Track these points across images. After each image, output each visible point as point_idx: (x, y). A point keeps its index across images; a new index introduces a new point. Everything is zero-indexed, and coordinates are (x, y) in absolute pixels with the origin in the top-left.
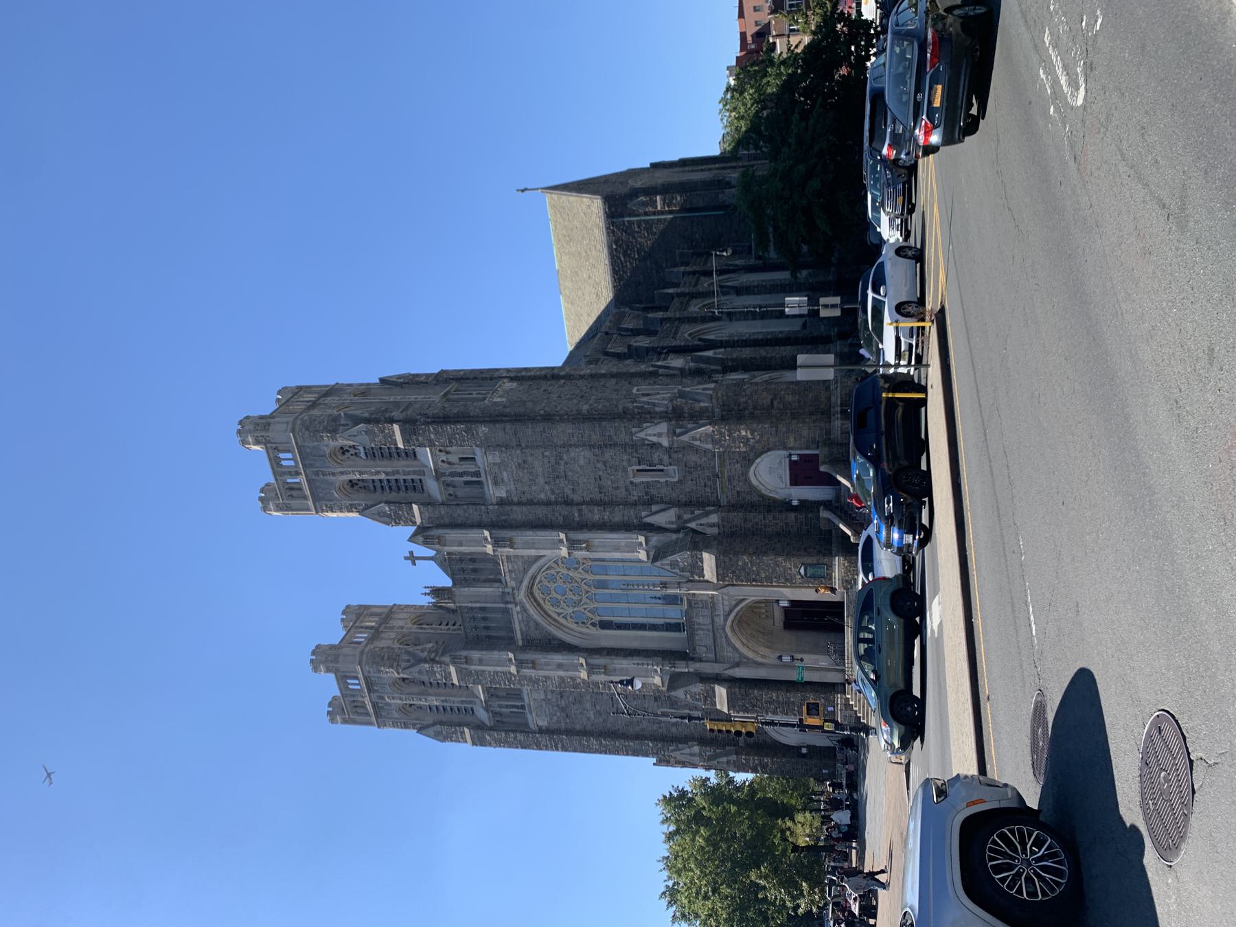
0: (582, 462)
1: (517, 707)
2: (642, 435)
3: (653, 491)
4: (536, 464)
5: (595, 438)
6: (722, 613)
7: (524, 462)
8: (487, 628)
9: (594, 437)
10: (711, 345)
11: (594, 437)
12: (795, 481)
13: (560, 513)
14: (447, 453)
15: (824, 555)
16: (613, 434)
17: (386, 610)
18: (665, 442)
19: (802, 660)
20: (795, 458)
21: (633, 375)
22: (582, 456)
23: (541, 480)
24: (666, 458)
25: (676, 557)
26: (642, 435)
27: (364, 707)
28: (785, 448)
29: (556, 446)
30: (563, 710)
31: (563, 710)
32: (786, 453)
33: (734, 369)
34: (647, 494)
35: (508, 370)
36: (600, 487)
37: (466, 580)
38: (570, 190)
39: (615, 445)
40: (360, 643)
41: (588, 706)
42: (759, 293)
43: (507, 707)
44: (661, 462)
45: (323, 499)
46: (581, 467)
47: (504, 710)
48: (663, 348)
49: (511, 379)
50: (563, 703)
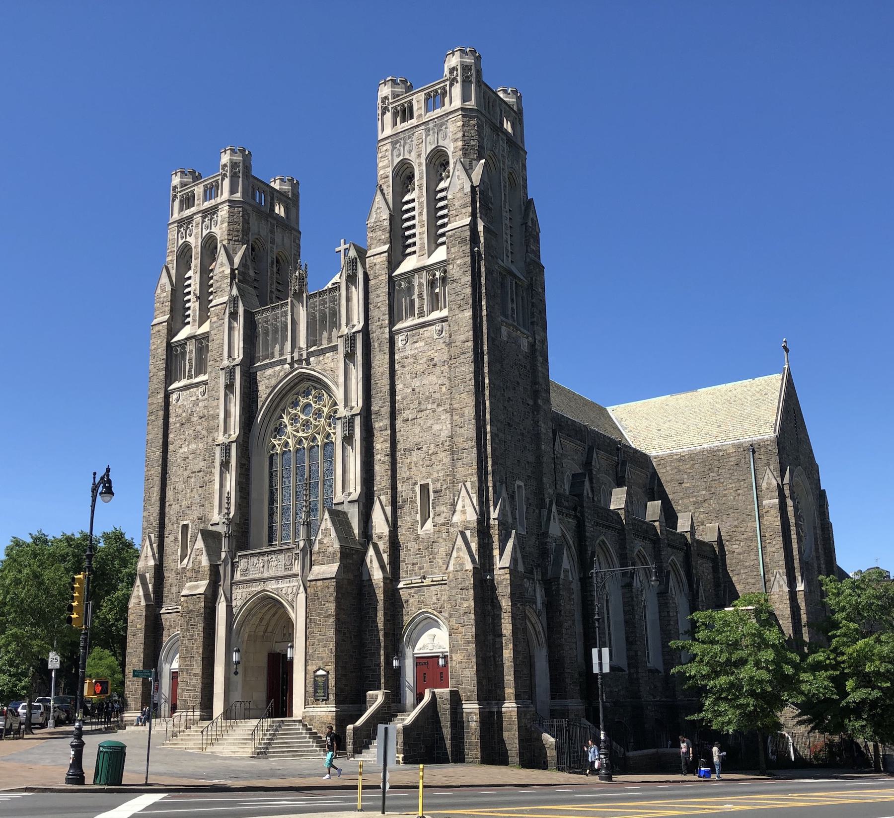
0: (436, 427)
2: (463, 493)
4: (433, 378)
7: (435, 365)
8: (266, 333)
10: (584, 563)
13: (380, 405)
16: (465, 461)
18: (457, 518)
19: (236, 673)
21: (540, 481)
22: (443, 428)
23: (416, 383)
25: (333, 534)
27: (188, 207)
30: (189, 420)
31: (189, 420)
33: (548, 592)
35: (544, 341)
38: (786, 401)
39: (454, 466)
40: (254, 198)
41: (193, 446)
42: (661, 618)
45: (394, 148)
49: (532, 346)
50: (194, 419)
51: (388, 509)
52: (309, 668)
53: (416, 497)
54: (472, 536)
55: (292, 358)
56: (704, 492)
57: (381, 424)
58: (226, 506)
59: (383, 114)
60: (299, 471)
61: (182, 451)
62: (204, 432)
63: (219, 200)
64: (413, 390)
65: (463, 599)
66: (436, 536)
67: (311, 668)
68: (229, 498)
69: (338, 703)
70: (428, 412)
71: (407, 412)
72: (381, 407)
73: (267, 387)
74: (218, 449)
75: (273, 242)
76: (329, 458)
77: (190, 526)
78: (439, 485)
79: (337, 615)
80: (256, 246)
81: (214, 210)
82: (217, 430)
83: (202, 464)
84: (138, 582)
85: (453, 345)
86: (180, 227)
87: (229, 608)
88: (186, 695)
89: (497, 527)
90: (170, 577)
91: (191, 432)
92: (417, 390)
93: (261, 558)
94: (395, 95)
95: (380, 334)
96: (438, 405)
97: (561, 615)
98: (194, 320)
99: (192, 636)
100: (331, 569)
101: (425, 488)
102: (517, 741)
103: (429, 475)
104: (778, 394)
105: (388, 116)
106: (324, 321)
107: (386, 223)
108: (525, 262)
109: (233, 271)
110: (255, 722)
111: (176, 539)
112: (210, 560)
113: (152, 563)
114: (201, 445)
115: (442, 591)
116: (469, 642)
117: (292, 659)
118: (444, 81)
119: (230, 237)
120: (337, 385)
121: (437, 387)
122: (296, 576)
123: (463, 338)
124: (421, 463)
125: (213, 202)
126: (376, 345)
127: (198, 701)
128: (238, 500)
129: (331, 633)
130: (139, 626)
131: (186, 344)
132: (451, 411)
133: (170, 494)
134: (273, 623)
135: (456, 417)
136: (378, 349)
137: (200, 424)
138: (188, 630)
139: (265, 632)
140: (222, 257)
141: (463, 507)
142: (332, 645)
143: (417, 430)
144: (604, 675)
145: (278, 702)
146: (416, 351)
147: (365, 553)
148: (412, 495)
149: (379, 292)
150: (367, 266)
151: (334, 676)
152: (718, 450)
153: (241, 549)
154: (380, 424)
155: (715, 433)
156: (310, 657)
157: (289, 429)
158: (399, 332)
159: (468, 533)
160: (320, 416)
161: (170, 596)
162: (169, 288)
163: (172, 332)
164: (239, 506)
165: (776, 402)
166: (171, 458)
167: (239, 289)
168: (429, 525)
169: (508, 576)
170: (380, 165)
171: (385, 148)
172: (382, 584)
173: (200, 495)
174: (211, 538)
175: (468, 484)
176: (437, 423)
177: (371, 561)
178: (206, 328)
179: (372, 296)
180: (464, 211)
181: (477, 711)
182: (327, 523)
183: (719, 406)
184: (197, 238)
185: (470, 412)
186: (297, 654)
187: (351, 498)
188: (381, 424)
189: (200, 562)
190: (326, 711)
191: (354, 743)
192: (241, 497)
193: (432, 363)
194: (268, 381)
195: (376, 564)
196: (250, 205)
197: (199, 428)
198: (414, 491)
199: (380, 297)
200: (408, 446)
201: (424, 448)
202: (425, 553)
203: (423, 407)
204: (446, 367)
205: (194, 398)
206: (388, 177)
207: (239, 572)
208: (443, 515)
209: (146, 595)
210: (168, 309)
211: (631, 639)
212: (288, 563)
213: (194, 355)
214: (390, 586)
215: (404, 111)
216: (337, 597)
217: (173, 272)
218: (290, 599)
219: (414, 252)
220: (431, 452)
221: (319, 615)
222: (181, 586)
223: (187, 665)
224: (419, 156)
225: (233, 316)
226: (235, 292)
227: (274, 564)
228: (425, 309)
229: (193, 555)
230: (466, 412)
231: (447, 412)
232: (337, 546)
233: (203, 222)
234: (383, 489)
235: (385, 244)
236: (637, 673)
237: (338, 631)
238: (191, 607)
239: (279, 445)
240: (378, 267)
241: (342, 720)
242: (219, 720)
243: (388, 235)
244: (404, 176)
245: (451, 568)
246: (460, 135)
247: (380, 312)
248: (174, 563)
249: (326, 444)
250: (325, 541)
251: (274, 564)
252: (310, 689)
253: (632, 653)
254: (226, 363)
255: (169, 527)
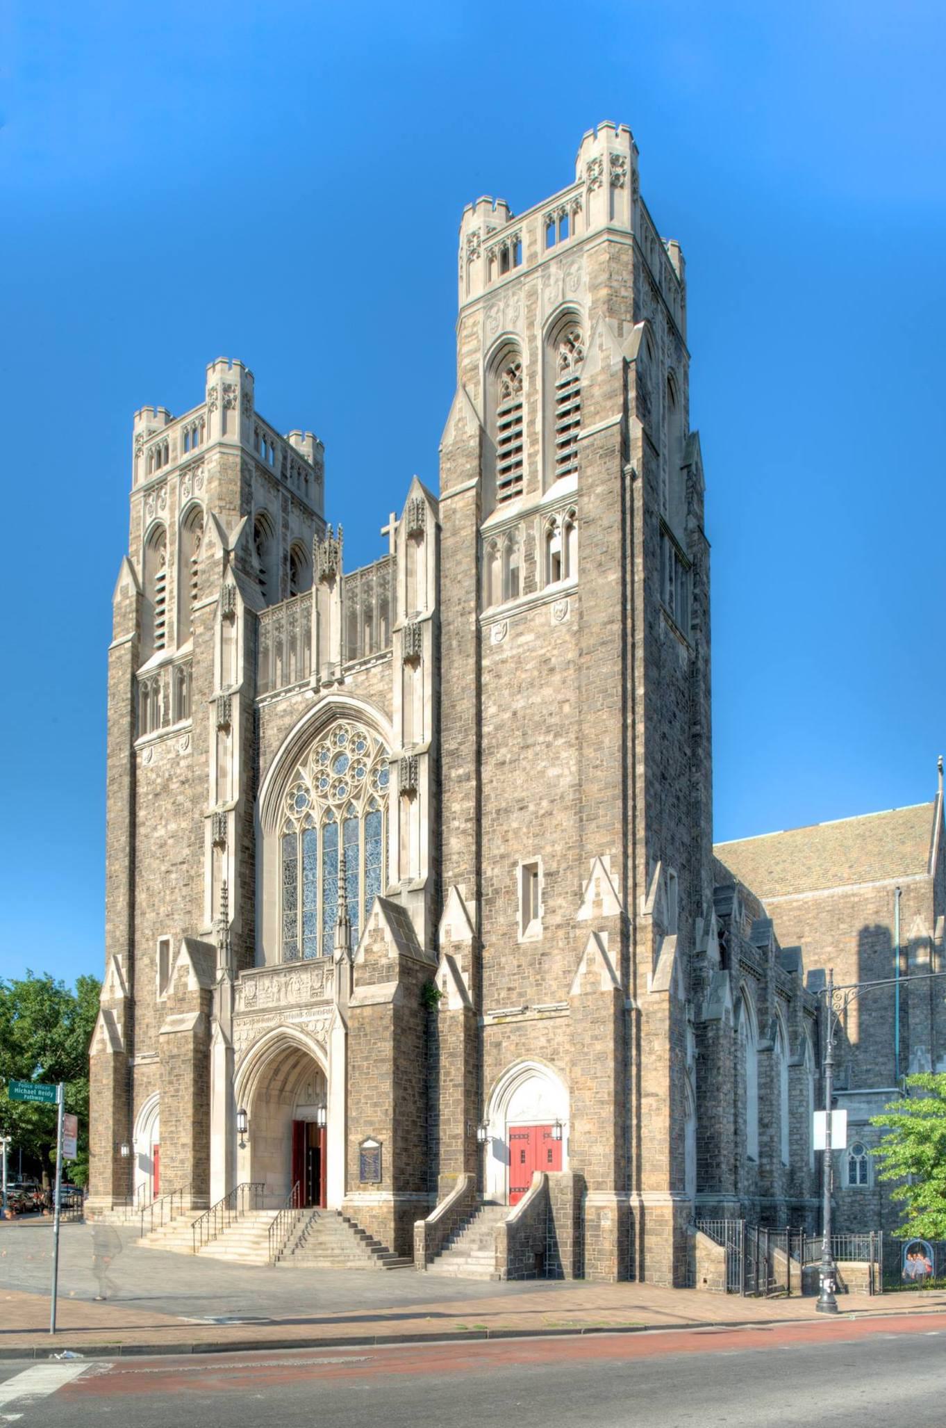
0: (552, 772)
1: (166, 713)
4: (548, 692)
5: (593, 789)
6: (304, 1019)
7: (552, 670)
9: (595, 787)
11: (595, 787)
12: (810, 973)
13: (458, 741)
14: (569, 528)
16: (602, 821)
17: (316, 509)
18: (586, 913)
20: (555, 1133)
22: (563, 772)
23: (519, 703)
24: (557, 919)
25: (388, 935)
26: (598, 872)
28: (573, 1116)
29: (580, 723)
30: (165, 788)
31: (165, 788)
34: (497, 892)
36: (507, 811)
41: (173, 826)
44: (551, 911)
46: (542, 773)
47: (161, 696)
48: (728, 941)
50: (174, 786)
51: (471, 906)
52: (351, 1137)
53: (515, 883)
54: (611, 940)
55: (318, 680)
56: (829, 949)
57: (461, 771)
58: (222, 901)
59: (470, 261)
60: (330, 860)
61: (156, 835)
62: (188, 805)
63: (205, 446)
64: (515, 714)
65: (595, 1038)
66: (548, 945)
68: (225, 890)
69: (399, 1188)
70: (538, 748)
72: (460, 744)
73: (279, 730)
74: (208, 823)
75: (286, 526)
78: (555, 865)
79: (395, 1059)
80: (261, 529)
82: (207, 799)
83: (186, 851)
84: (101, 1020)
85: (586, 631)
86: (147, 496)
87: (230, 1051)
88: (170, 1173)
89: (650, 928)
90: (144, 1014)
91: (169, 806)
92: (520, 714)
93: (276, 978)
94: (491, 230)
95: (460, 623)
96: (555, 736)
98: (171, 638)
99: (177, 1091)
100: (387, 990)
102: (670, 1250)
103: (537, 850)
105: (479, 265)
106: (370, 616)
107: (474, 443)
108: (686, 529)
109: (227, 553)
110: (274, 1213)
111: (152, 961)
112: (200, 982)
113: (120, 994)
114: (184, 825)
115: (554, 1027)
116: (602, 1102)
117: (325, 1127)
118: (578, 186)
119: (223, 503)
120: (389, 716)
121: (554, 708)
122: (328, 1003)
123: (603, 617)
124: (525, 830)
127: (189, 1180)
128: (240, 900)
129: (387, 1086)
130: (105, 1082)
131: (159, 674)
132: (580, 742)
133: (141, 897)
134: (292, 1079)
136: (456, 651)
137: (182, 793)
138: (171, 1083)
139: (282, 1090)
140: (211, 534)
141: (598, 895)
143: (519, 777)
145: (306, 1181)
146: (521, 650)
147: (434, 971)
148: (508, 882)
150: (441, 516)
151: (390, 1150)
153: (243, 966)
154: (458, 771)
156: (352, 1122)
158: (493, 620)
159: (604, 936)
160: (360, 773)
161: (147, 1041)
162: (132, 591)
163: (137, 659)
164: (240, 910)
165: (927, 837)
166: (141, 845)
167: (237, 578)
168: (536, 926)
169: (666, 1005)
172: (462, 1018)
173: (184, 897)
174: (201, 954)
175: (607, 860)
176: (553, 765)
177: (445, 983)
178: (188, 647)
179: (447, 565)
182: (379, 920)
183: (850, 842)
184: (172, 510)
185: (612, 740)
186: (332, 1118)
187: (413, 887)
188: (461, 771)
189: (185, 985)
191: (427, 1247)
192: (244, 896)
194: (285, 711)
195: (452, 988)
196: (253, 458)
197: (180, 798)
198: (513, 879)
199: (461, 565)
200: (504, 805)
201: (532, 808)
202: (529, 972)
203: (530, 741)
204: (571, 671)
205: (172, 755)
206: (476, 367)
207: (242, 1001)
208: (560, 912)
209: (114, 1039)
210: (132, 624)
211: (766, 1121)
212: (317, 985)
213: (171, 690)
214: (472, 1021)
215: (505, 255)
217: (139, 568)
218: (320, 1038)
219: (519, 493)
220: (542, 812)
221: (367, 1058)
222: (160, 1023)
223: (172, 1132)
224: (531, 325)
225: (229, 617)
226: (230, 580)
228: (537, 579)
229: (175, 976)
230: (607, 740)
231: (571, 746)
233: (182, 483)
234: (461, 875)
235: (471, 477)
236: (772, 1163)
237: (397, 1084)
238: (175, 1051)
239: (298, 819)
240: (458, 516)
241: (404, 1217)
242: (219, 1208)
243: (476, 463)
244: (503, 358)
245: (576, 990)
246: (604, 277)
248: (150, 992)
250: (376, 948)
251: (296, 987)
252: (355, 1169)
253: (766, 1139)
254: (218, 692)
255: (142, 945)
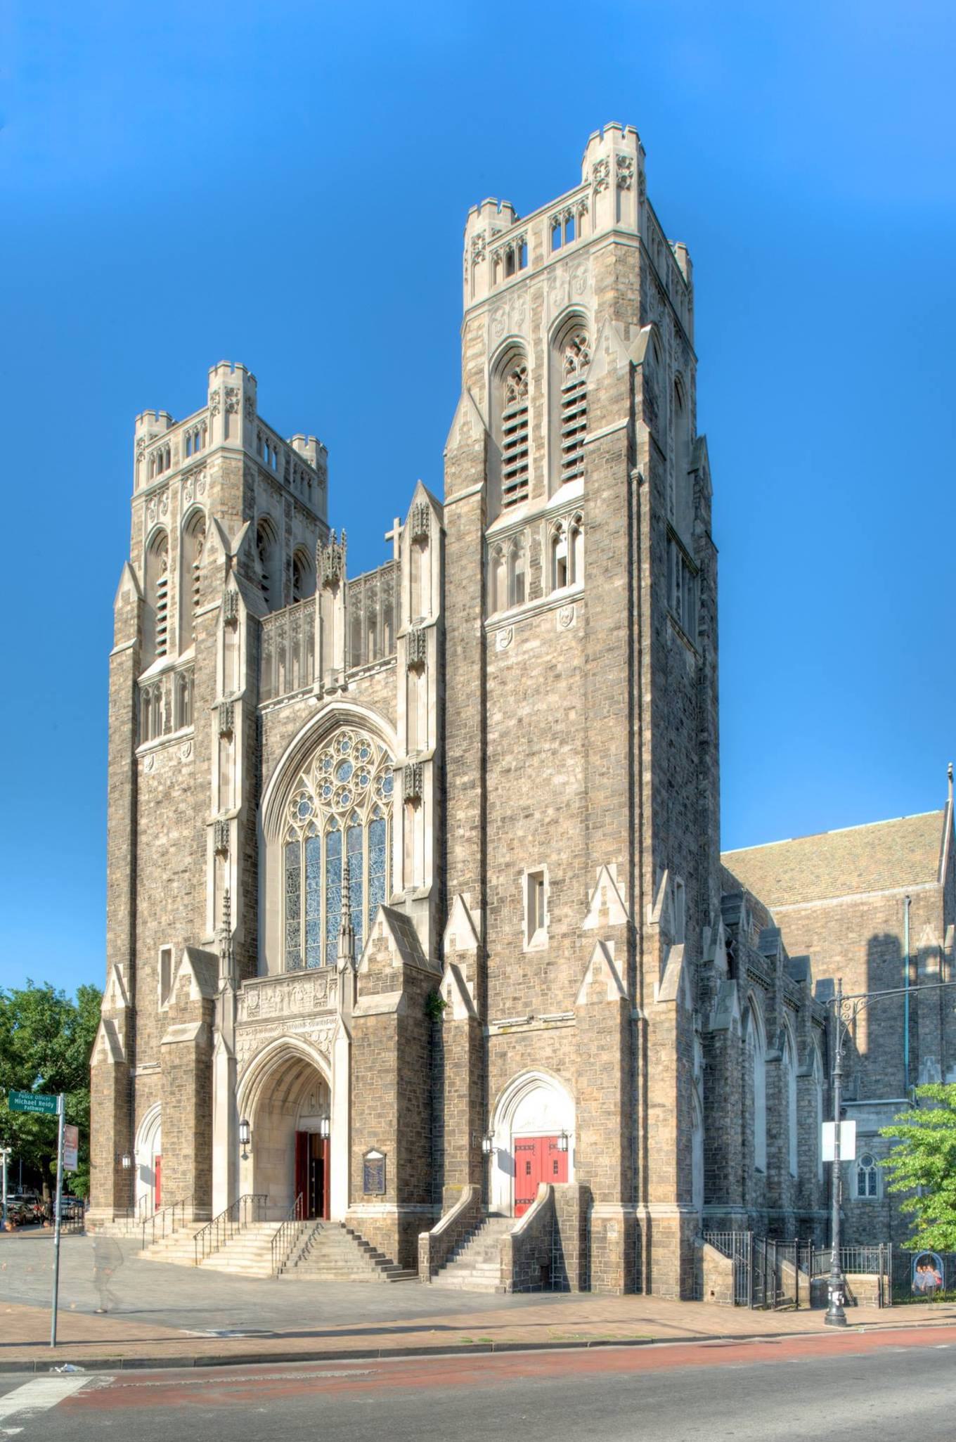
0: (558, 780)
1: (168, 720)
2: (604, 880)
3: (505, 911)
4: (553, 698)
5: (599, 797)
6: (307, 1029)
7: (558, 677)
14: (575, 533)
15: (400, 1190)
16: (608, 829)
17: (319, 514)
18: (592, 922)
20: (561, 1144)
22: (568, 778)
23: (524, 710)
24: (563, 928)
25: (392, 945)
26: (604, 880)
29: (586, 730)
30: (167, 795)
31: (167, 795)
32: (571, 1129)
34: (502, 900)
35: (714, 668)
36: (512, 819)
37: (356, 604)
39: (588, 837)
41: (174, 835)
43: (168, 704)
46: (548, 781)
47: (163, 703)
48: (736, 950)
50: (176, 793)
51: (476, 914)
52: (355, 1148)
53: (520, 892)
55: (322, 687)
57: (466, 779)
58: (224, 910)
59: (475, 263)
60: (333, 869)
61: (158, 843)
62: (190, 813)
63: (207, 451)
64: (520, 721)
65: (602, 1048)
66: (554, 954)
67: (358, 1149)
68: (227, 899)
69: (403, 1199)
70: (543, 755)
71: (509, 758)
72: (465, 751)
73: (282, 737)
74: (210, 831)
75: (289, 531)
76: (379, 841)
77: (173, 952)
78: (560, 873)
79: (399, 1070)
80: (264, 534)
81: (201, 466)
82: (209, 806)
83: (188, 860)
84: (102, 1030)
86: (148, 501)
87: (232, 1061)
88: (172, 1185)
89: (657, 937)
90: (145, 1024)
91: (171, 814)
92: (525, 721)
93: (278, 988)
94: (496, 233)
95: (465, 629)
96: (561, 743)
97: (726, 1084)
98: (173, 645)
99: (179, 1101)
100: (391, 1000)
101: (536, 879)
103: (543, 858)
104: (938, 835)
105: (484, 268)
106: (373, 623)
108: (693, 534)
109: (229, 558)
110: (277, 1225)
113: (121, 1004)
114: (186, 833)
115: (560, 1038)
117: (328, 1139)
119: (225, 508)
120: (393, 723)
122: (331, 1012)
123: (610, 623)
124: (530, 838)
125: (198, 456)
126: (459, 650)
128: (242, 909)
129: (391, 1097)
130: (106, 1092)
131: (160, 681)
132: (586, 750)
133: (143, 906)
134: (296, 1088)
135: (595, 759)
137: (184, 801)
138: (172, 1093)
139: (285, 1101)
140: (213, 540)
141: (604, 903)
142: (392, 1114)
143: (525, 785)
144: (844, 1165)
145: (309, 1194)
146: (526, 656)
147: (439, 981)
148: (513, 890)
149: (464, 562)
150: (446, 521)
151: (395, 1161)
152: (862, 904)
153: (245, 975)
154: (462, 779)
155: (854, 884)
156: (356, 1133)
157: (317, 803)
158: (498, 626)
159: (611, 945)
160: (364, 780)
162: (134, 597)
164: (243, 918)
165: (937, 845)
166: (143, 853)
168: (541, 936)
169: (673, 1015)
170: (470, 353)
171: (476, 324)
172: (466, 1028)
173: (186, 906)
174: (204, 963)
175: (613, 868)
176: (559, 773)
177: (449, 992)
178: (190, 653)
179: (452, 570)
180: (615, 407)
181: (621, 1216)
182: (383, 928)
183: (859, 851)
184: (174, 515)
185: (618, 748)
186: (335, 1129)
188: (466, 779)
189: (187, 995)
190: (382, 1212)
192: (246, 905)
193: (552, 674)
196: (256, 463)
197: (182, 806)
198: (519, 887)
199: (466, 571)
201: (537, 815)
202: (535, 981)
203: (536, 748)
204: (578, 678)
205: (174, 763)
206: (481, 371)
207: (245, 1011)
208: (566, 921)
209: (115, 1049)
211: (774, 1132)
212: (320, 995)
214: (477, 1031)
216: (399, 1043)
217: (140, 574)
218: (323, 1048)
219: (525, 497)
220: (547, 820)
221: (371, 1069)
222: (162, 1033)
223: (173, 1143)
224: (536, 328)
226: (233, 586)
227: (299, 996)
228: (543, 585)
231: (577, 753)
232: (398, 963)
233: (183, 488)
234: (466, 883)
235: (476, 482)
236: (780, 1175)
237: (401, 1095)
238: (177, 1062)
239: (301, 827)
240: (463, 521)
241: (408, 1229)
242: (221, 1220)
243: (481, 467)
244: (509, 361)
246: (610, 280)
247: (465, 596)
248: (151, 1001)
249: (372, 822)
250: (380, 957)
251: (299, 996)
252: (358, 1180)
253: (774, 1150)
255: (143, 954)
